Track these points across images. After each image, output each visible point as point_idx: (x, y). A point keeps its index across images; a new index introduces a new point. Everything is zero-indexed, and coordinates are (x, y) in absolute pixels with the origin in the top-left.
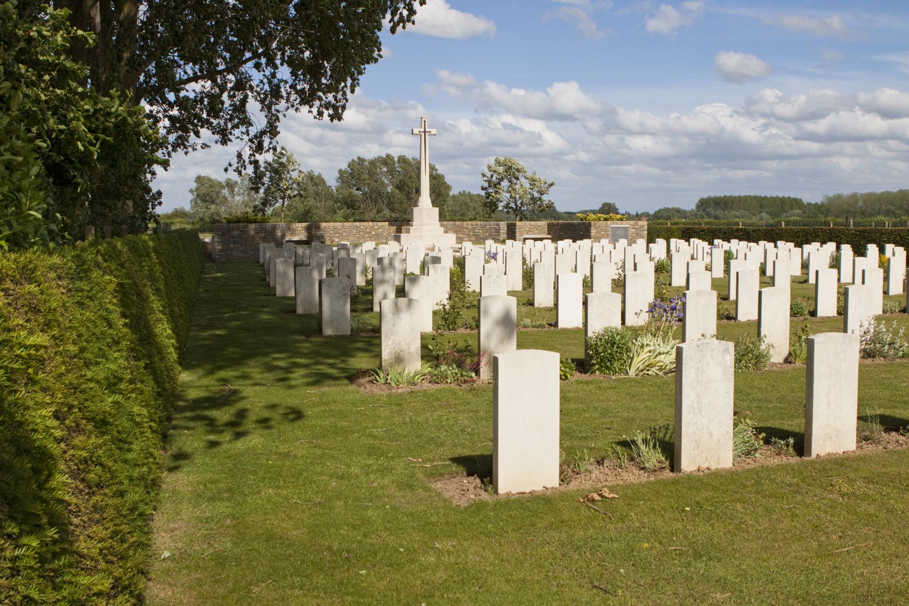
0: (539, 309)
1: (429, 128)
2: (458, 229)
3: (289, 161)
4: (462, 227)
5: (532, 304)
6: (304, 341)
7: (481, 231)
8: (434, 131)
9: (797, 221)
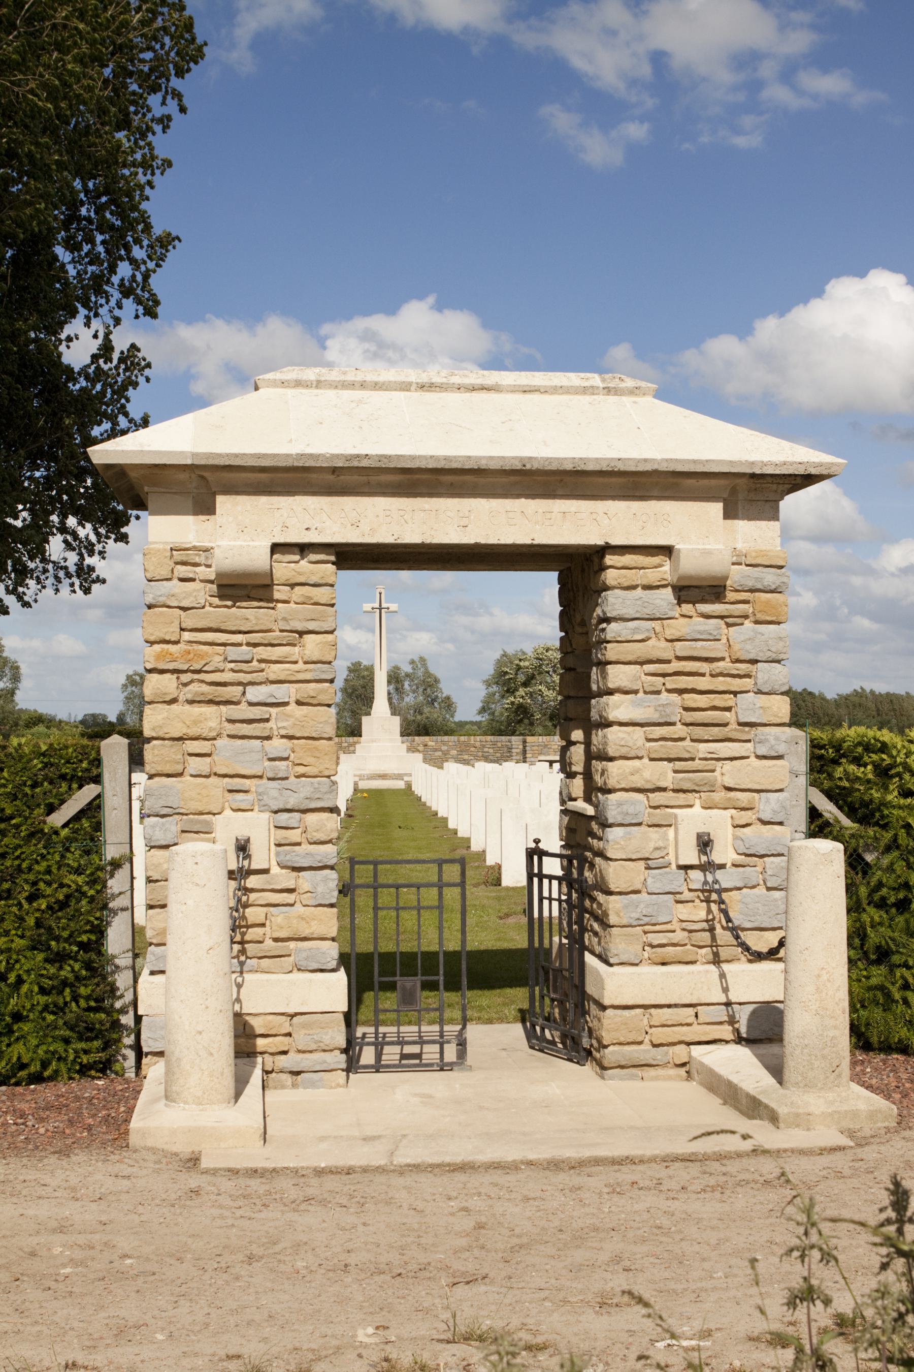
0: (508, 889)
1: (386, 602)
2: (463, 747)
3: (100, 553)
4: (468, 745)
5: (498, 882)
6: (99, 1078)
7: (491, 751)
8: (393, 607)
9: (350, 837)
